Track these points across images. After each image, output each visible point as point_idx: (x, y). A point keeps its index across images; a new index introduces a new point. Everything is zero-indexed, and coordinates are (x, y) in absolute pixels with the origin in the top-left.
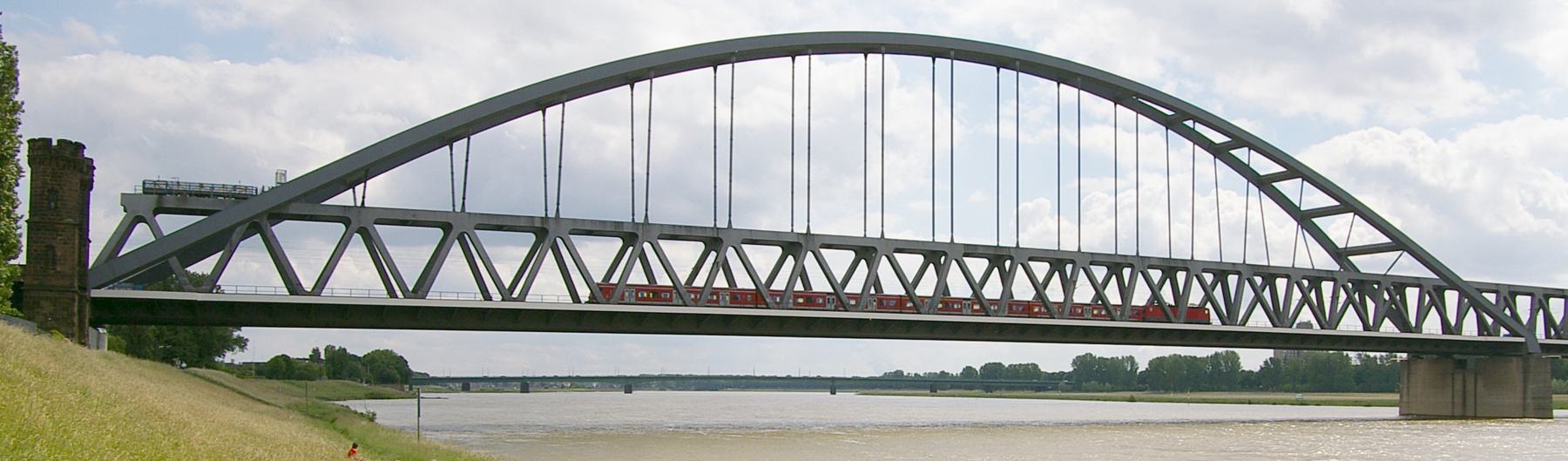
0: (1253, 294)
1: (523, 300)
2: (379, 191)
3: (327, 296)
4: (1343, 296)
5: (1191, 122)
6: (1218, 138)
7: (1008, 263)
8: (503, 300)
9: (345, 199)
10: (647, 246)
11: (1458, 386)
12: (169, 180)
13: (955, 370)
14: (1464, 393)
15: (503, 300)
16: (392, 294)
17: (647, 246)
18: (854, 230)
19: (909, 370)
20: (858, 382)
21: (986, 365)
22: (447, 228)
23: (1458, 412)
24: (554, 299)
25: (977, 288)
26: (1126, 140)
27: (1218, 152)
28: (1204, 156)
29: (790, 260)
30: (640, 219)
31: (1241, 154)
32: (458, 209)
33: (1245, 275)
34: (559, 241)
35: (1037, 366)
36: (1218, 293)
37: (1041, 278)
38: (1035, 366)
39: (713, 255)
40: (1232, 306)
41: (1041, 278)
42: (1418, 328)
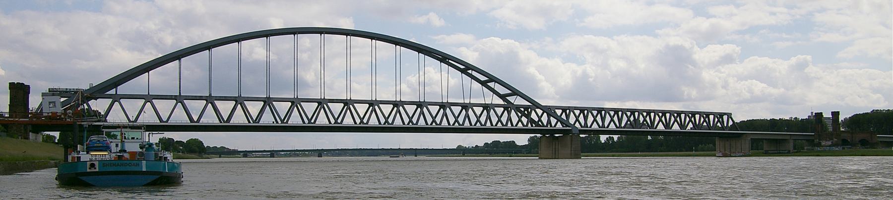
0: (659, 119)
1: (441, 125)
2: (122, 89)
3: (141, 121)
4: (716, 120)
5: (471, 71)
6: (483, 78)
7: (529, 110)
8: (281, 123)
9: (113, 92)
10: (351, 106)
11: (554, 147)
12: (56, 88)
13: (481, 144)
14: (555, 149)
15: (281, 123)
16: (249, 122)
17: (351, 106)
18: (461, 101)
19: (466, 145)
20: (384, 151)
21: (493, 142)
22: (236, 101)
23: (554, 157)
24: (399, 124)
25: (540, 118)
26: (445, 74)
27: (483, 83)
28: (476, 86)
29: (396, 108)
30: (374, 99)
31: (491, 84)
32: (296, 97)
33: (702, 115)
34: (298, 105)
35: (514, 142)
36: (648, 119)
37: (612, 115)
38: (514, 142)
39: (371, 108)
40: (652, 123)
41: (612, 115)
42: (591, 127)
